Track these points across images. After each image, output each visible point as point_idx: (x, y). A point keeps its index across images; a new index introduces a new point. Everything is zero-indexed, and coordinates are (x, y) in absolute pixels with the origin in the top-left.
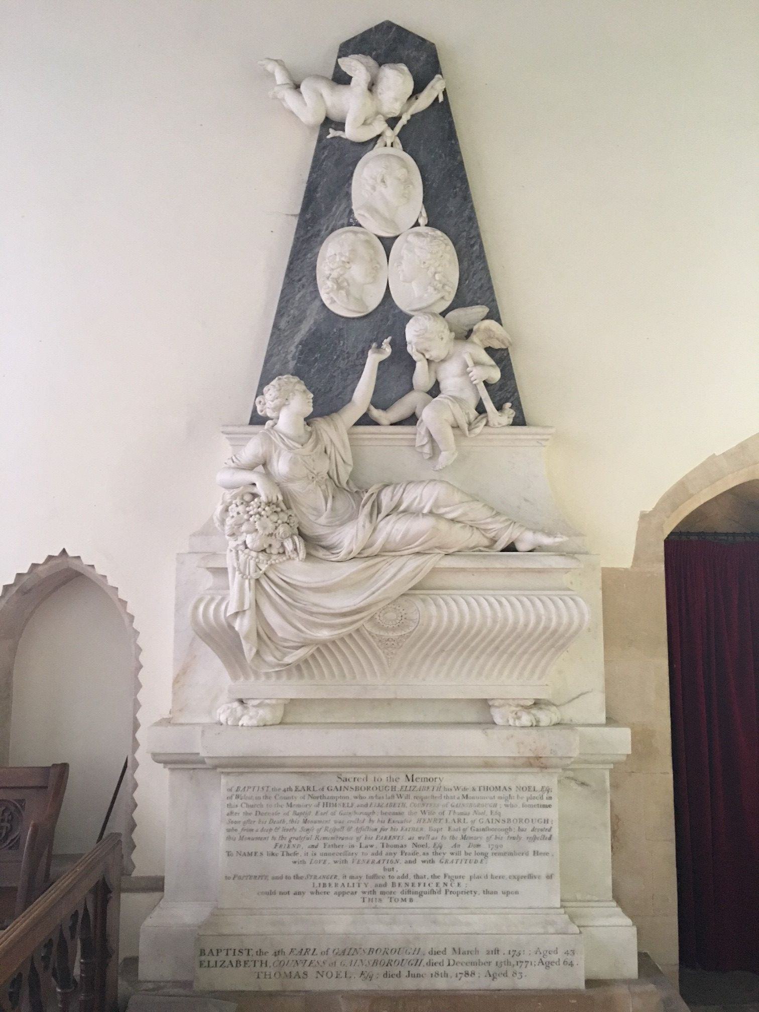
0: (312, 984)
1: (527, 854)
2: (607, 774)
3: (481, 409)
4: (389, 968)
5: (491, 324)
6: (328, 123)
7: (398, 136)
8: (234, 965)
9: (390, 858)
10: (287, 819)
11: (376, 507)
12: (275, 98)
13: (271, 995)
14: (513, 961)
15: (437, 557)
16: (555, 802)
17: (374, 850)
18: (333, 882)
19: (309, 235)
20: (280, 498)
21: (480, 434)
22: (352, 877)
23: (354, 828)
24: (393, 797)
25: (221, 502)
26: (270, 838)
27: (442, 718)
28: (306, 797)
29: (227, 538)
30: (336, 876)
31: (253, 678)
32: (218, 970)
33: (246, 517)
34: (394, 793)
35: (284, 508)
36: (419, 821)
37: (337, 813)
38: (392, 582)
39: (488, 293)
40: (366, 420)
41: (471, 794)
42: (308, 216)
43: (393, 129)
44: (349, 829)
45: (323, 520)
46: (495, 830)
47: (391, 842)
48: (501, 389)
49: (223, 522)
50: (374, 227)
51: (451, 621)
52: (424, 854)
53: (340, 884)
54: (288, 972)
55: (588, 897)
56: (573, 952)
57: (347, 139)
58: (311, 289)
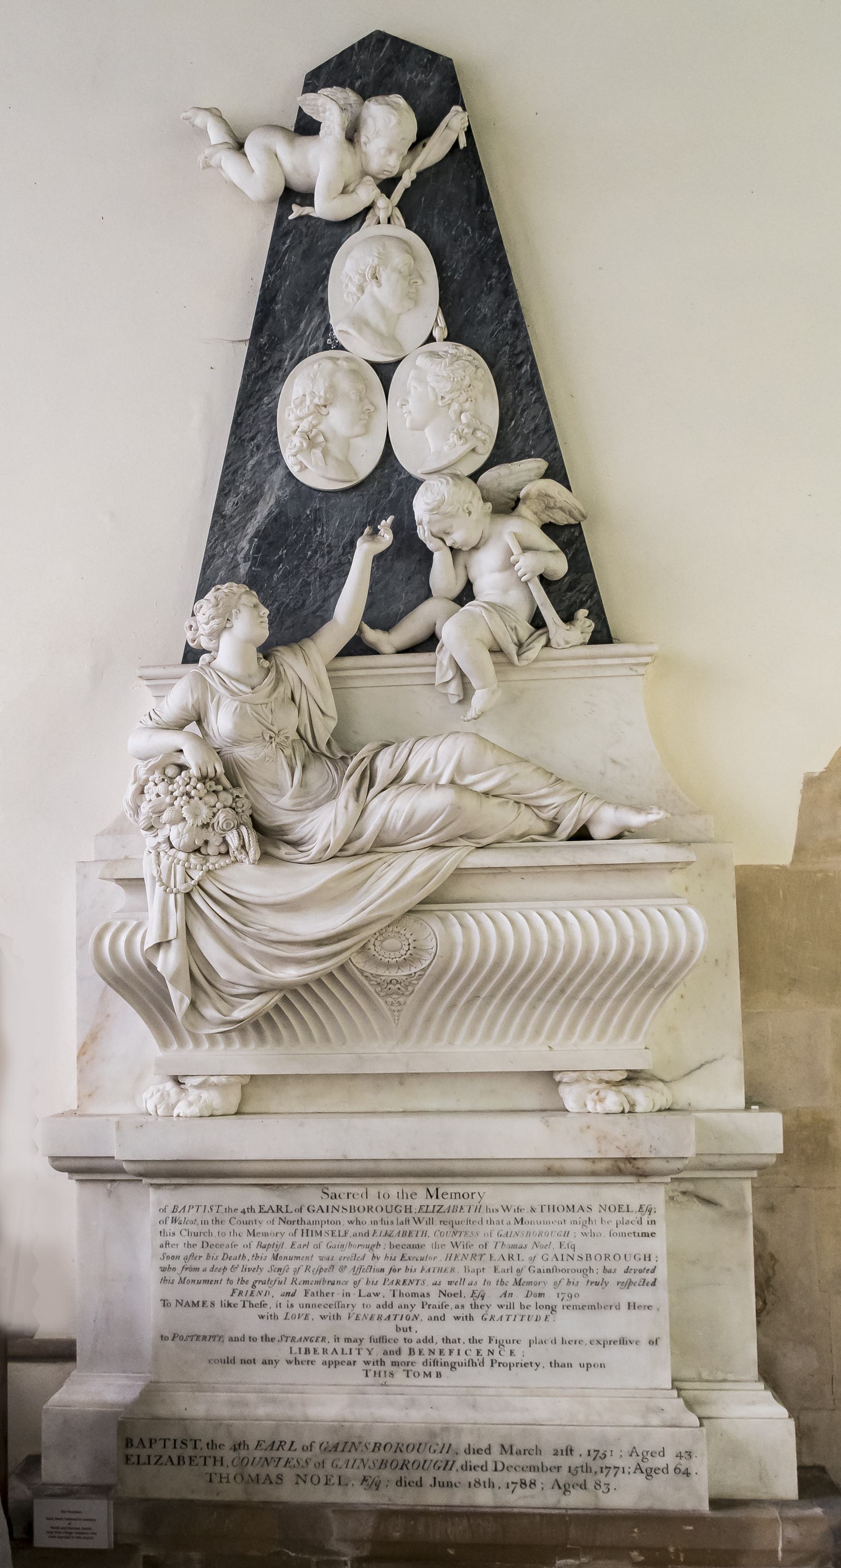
0: (289, 1493)
1: (618, 1307)
2: (747, 1186)
3: (537, 622)
4: (403, 1473)
5: (552, 487)
6: (292, 195)
7: (399, 206)
8: (175, 1461)
9: (405, 1312)
10: (249, 1253)
11: (368, 777)
12: (207, 166)
13: (230, 1507)
14: (595, 1466)
15: (463, 852)
16: (661, 1228)
17: (380, 1301)
18: (320, 1346)
19: (266, 368)
20: (220, 769)
21: (536, 660)
22: (348, 1340)
23: (350, 1268)
24: (407, 1221)
25: (132, 779)
26: (224, 1281)
27: (483, 1105)
28: (277, 1221)
29: (144, 832)
30: (324, 1339)
31: (190, 1045)
32: (151, 1469)
33: (168, 799)
34: (410, 1216)
35: (228, 784)
36: (449, 1257)
37: (323, 1246)
38: (393, 891)
39: (547, 439)
40: (357, 647)
41: (528, 1216)
42: (262, 341)
43: (389, 196)
44: (342, 1269)
45: (286, 801)
46: (567, 1271)
47: (405, 1289)
48: (571, 588)
49: (136, 810)
50: (363, 348)
51: (485, 951)
52: (457, 1307)
53: (330, 1351)
54: (253, 1475)
55: (720, 1376)
56: (689, 1454)
57: (319, 219)
58: (270, 450)
